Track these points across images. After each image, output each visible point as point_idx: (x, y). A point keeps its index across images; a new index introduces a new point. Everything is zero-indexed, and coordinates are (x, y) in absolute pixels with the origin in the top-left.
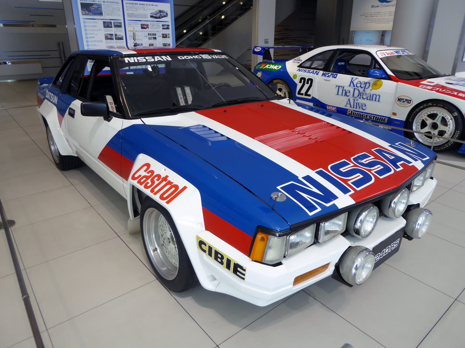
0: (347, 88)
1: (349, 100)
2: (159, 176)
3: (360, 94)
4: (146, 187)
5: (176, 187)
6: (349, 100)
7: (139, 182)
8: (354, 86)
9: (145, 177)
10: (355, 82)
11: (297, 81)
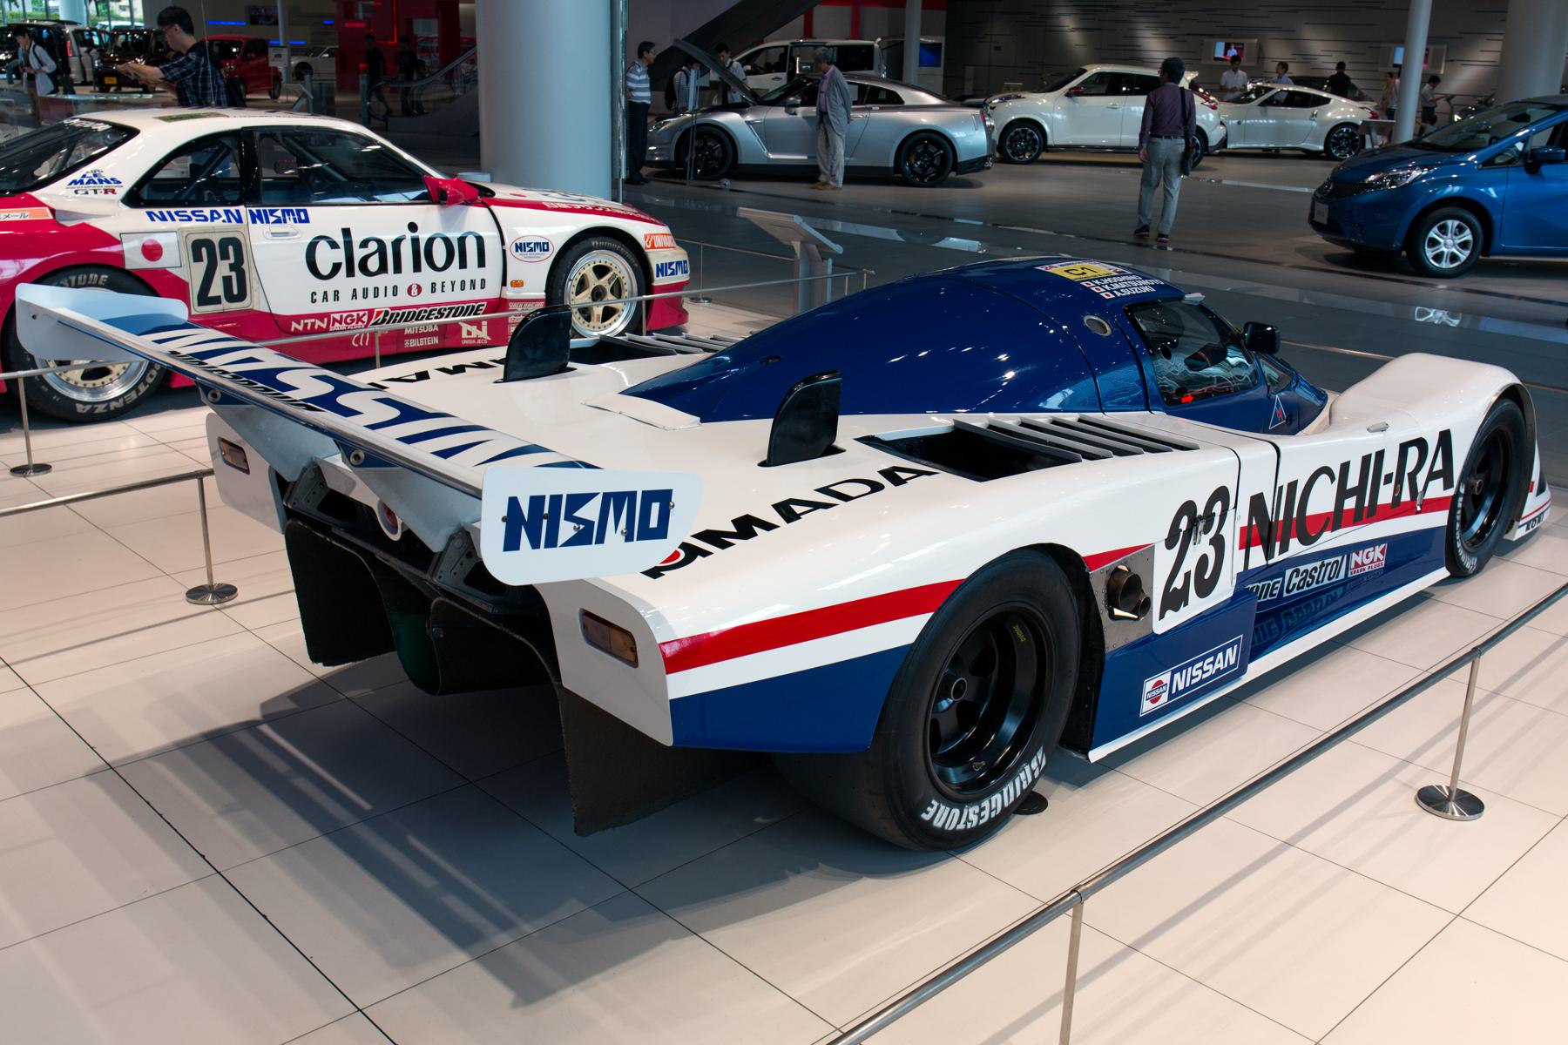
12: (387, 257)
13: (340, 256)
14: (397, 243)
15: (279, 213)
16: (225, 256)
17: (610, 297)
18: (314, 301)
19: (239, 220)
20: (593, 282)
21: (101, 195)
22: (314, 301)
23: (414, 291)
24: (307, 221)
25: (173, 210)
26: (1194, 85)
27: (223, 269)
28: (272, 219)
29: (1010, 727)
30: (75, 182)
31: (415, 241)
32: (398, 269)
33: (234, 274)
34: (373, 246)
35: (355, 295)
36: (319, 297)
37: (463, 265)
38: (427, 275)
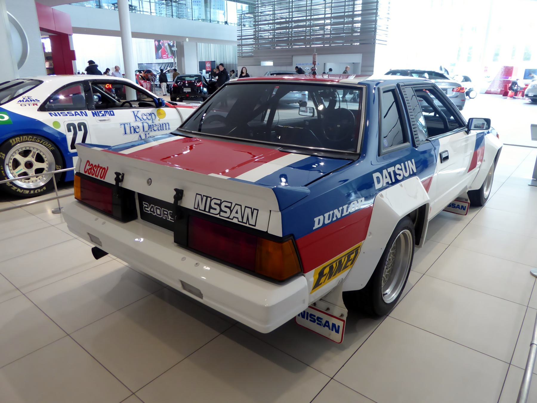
0: (134, 124)
1: (140, 136)
2: (95, 166)
3: (150, 126)
4: (93, 175)
5: (104, 168)
6: (140, 136)
7: (89, 173)
8: (141, 120)
9: (90, 169)
10: (139, 115)
11: (63, 129)
15: (103, 112)
19: (86, 115)
20: (22, 160)
21: (32, 106)
24: (114, 115)
25: (59, 112)
26: (357, 32)
28: (101, 115)
30: (20, 101)
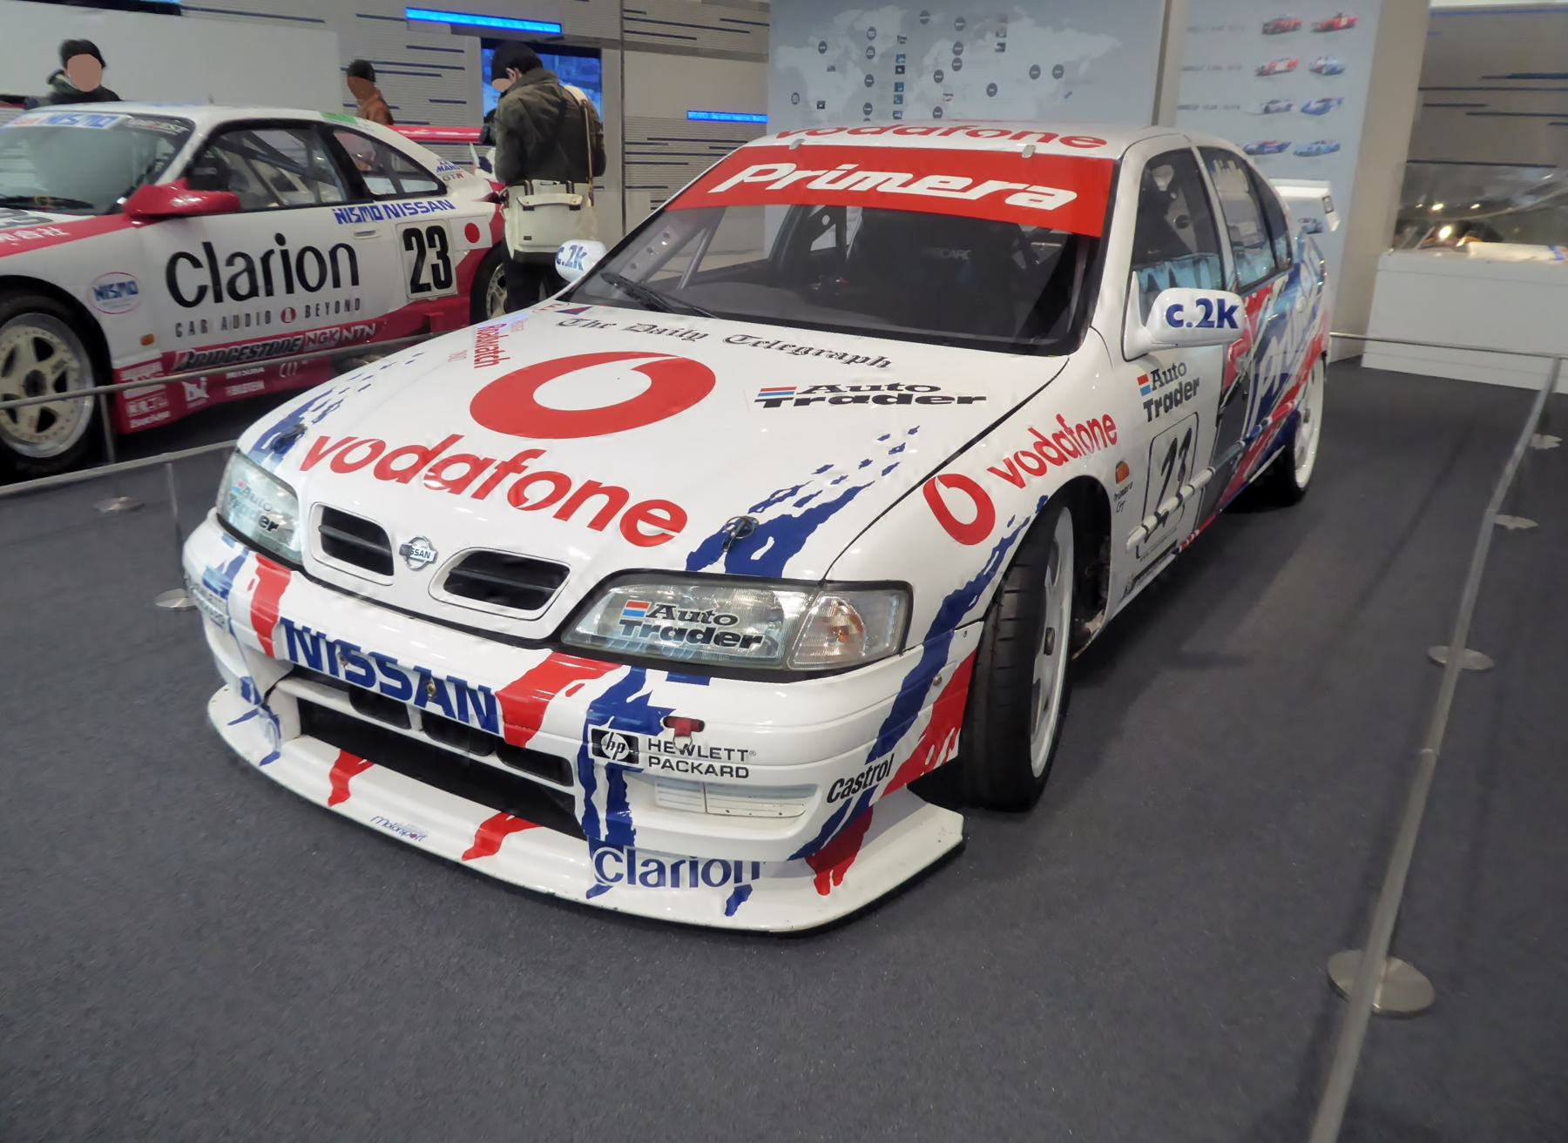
12: (258, 275)
13: (203, 276)
14: (266, 259)
15: (357, 212)
16: (432, 245)
17: (51, 393)
18: (179, 334)
22: (179, 334)
23: (288, 315)
27: (432, 256)
28: (354, 218)
29: (1517, 230)
31: (285, 254)
32: (269, 293)
33: (440, 262)
34: (240, 264)
35: (224, 326)
36: (185, 329)
37: (337, 284)
38: (301, 296)
